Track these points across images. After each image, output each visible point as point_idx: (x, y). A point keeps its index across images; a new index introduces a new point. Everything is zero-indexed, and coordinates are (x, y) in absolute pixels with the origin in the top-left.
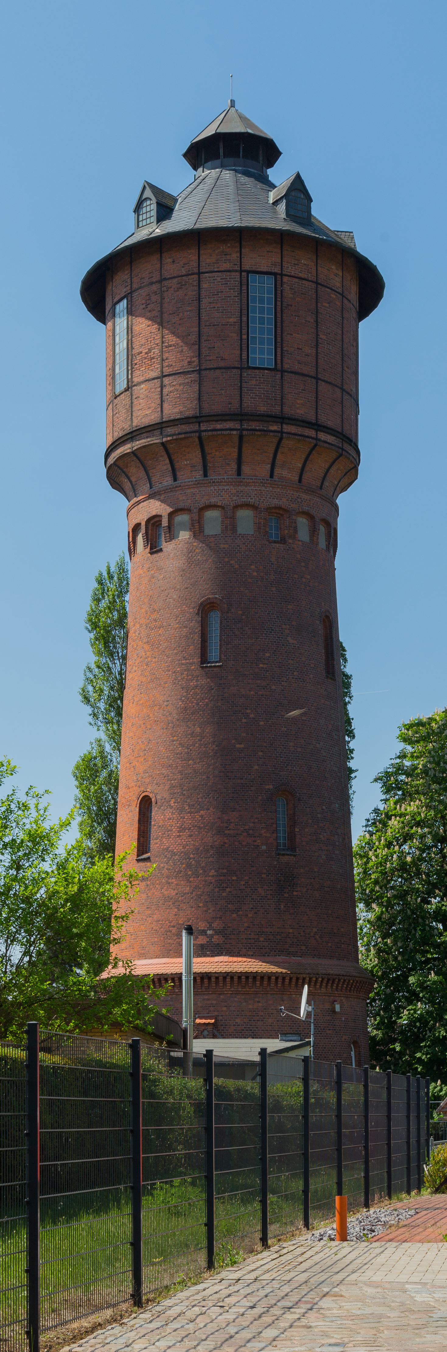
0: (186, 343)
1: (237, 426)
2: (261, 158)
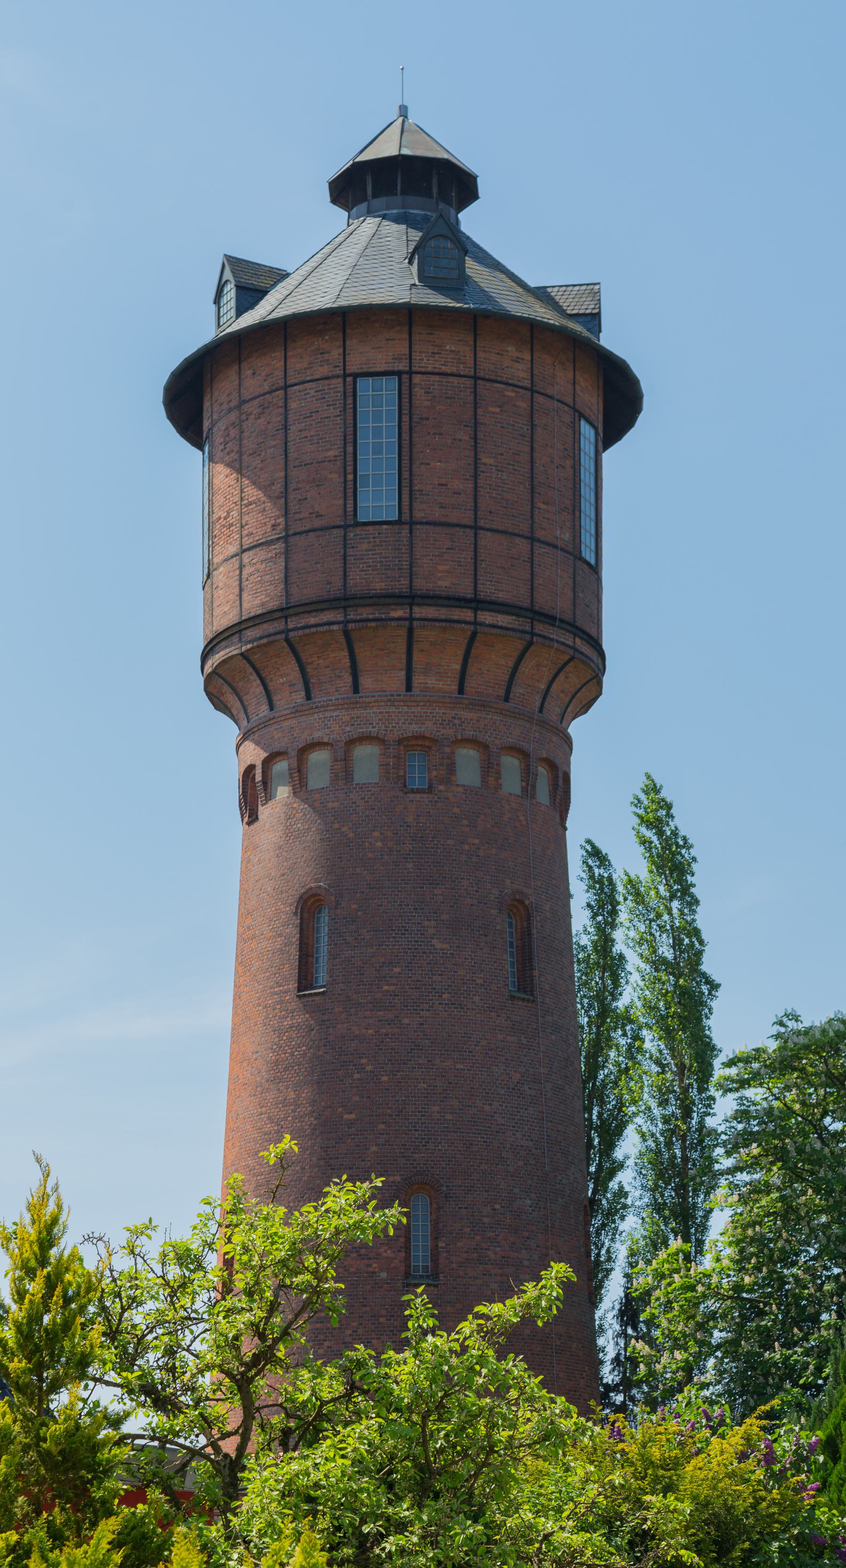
0: (269, 497)
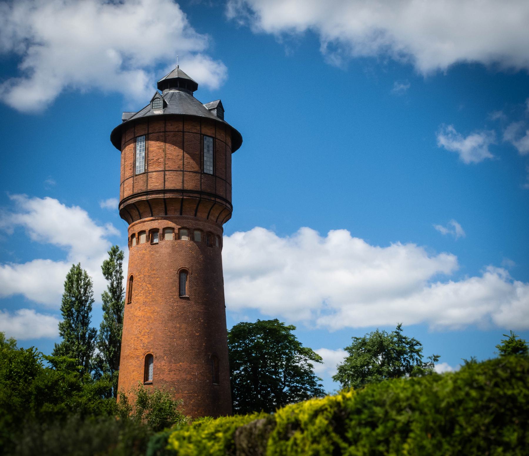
1: (199, 196)
2: (178, 85)
